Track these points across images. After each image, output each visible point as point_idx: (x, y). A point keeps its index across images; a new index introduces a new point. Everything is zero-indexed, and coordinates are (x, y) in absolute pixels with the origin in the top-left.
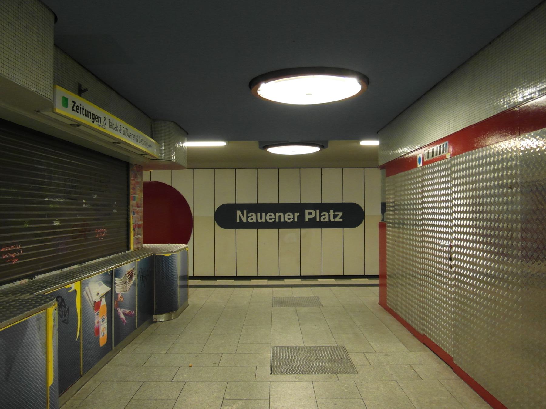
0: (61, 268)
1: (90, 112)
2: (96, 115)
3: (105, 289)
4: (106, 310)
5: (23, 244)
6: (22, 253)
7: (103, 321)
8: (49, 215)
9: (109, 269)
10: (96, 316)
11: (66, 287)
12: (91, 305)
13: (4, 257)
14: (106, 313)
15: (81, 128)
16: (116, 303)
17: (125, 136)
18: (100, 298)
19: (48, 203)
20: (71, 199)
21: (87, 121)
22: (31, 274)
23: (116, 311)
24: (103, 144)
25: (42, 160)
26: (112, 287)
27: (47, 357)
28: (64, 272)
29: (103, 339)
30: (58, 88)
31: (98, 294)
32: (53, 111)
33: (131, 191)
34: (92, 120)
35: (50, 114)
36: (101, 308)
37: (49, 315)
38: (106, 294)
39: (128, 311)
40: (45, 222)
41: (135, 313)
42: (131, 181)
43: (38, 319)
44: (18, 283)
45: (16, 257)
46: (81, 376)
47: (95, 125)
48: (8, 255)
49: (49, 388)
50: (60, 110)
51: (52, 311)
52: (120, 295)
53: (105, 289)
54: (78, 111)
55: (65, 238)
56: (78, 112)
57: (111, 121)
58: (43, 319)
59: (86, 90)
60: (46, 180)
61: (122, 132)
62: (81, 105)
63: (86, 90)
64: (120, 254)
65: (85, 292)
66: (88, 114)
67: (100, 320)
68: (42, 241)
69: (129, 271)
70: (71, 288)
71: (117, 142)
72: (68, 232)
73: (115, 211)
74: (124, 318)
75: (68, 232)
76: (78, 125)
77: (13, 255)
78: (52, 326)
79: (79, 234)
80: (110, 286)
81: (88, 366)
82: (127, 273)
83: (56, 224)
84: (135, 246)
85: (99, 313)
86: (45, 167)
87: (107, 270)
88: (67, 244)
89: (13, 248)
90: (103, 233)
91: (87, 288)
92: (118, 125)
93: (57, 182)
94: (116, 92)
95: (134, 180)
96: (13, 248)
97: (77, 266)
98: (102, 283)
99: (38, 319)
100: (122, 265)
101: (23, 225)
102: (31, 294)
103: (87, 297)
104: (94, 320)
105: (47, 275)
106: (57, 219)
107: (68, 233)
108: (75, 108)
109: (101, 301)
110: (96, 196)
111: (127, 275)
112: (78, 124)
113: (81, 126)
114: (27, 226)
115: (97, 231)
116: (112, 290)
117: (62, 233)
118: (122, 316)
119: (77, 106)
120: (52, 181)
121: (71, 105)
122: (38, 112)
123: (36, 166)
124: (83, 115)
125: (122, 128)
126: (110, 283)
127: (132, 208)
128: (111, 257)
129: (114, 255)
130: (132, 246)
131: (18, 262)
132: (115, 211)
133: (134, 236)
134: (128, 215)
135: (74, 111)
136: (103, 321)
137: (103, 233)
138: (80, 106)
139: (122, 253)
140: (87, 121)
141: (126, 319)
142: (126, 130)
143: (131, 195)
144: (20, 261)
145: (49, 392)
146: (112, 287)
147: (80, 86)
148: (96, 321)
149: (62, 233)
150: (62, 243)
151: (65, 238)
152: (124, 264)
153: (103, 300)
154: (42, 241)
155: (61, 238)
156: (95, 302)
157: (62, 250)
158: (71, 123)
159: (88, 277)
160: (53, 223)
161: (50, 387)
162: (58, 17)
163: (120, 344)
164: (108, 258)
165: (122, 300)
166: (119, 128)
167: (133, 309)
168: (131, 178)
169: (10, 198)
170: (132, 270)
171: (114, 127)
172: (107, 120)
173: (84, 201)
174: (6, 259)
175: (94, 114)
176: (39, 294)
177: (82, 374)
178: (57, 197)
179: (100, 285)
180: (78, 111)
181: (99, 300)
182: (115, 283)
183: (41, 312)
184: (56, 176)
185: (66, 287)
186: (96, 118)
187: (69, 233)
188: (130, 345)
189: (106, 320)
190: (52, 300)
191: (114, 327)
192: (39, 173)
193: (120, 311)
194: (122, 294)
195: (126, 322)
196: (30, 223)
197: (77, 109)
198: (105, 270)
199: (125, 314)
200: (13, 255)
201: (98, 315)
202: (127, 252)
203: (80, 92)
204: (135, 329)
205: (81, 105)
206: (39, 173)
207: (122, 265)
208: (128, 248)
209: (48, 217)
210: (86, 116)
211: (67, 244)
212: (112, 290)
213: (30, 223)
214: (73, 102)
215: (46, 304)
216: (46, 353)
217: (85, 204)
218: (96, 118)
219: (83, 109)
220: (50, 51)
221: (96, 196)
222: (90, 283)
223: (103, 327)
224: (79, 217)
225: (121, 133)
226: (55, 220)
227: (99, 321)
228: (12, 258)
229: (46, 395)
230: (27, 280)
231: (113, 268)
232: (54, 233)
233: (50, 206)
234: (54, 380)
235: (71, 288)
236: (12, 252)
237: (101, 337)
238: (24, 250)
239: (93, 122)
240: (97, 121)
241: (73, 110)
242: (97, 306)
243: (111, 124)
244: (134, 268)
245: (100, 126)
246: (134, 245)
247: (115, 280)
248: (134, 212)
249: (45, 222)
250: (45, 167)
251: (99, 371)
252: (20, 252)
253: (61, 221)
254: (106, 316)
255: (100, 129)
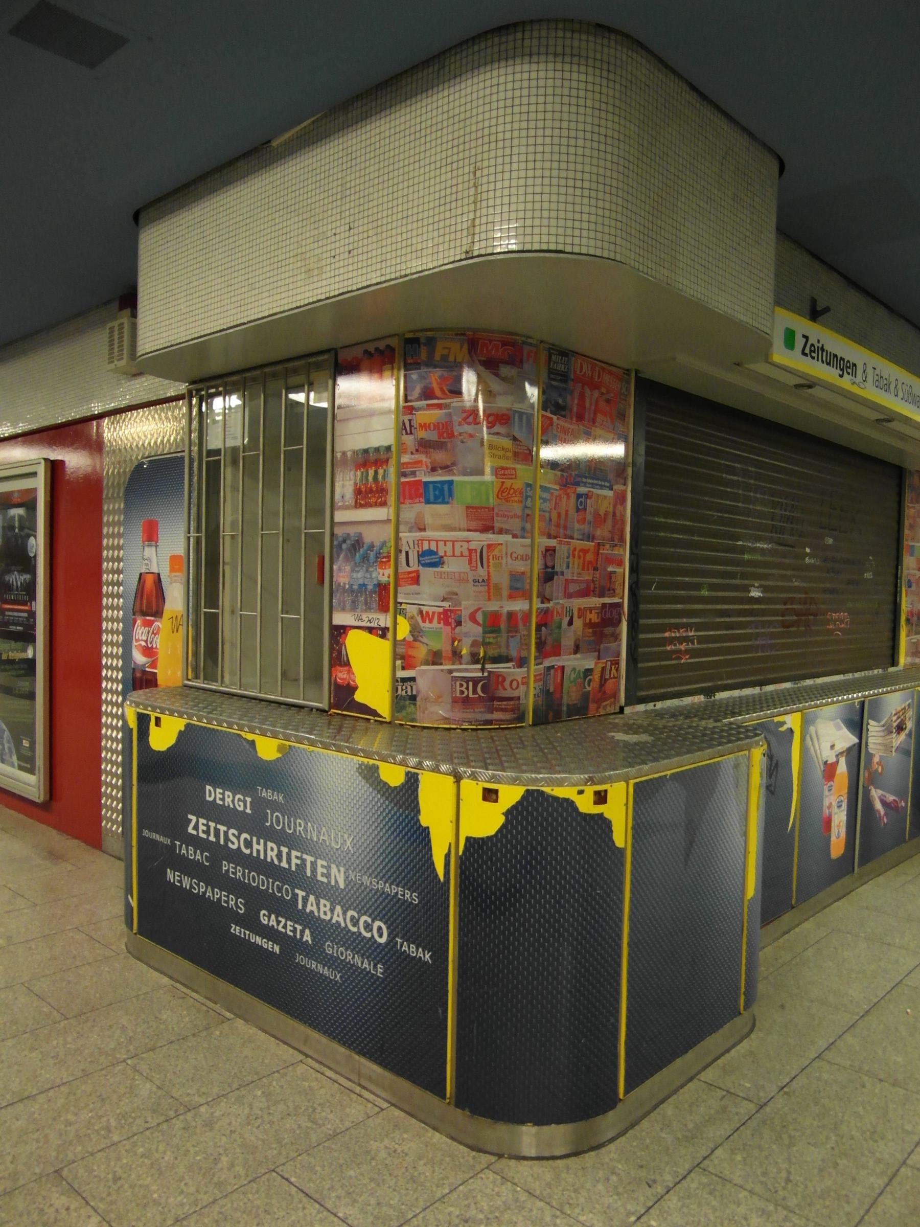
0: (761, 684)
1: (835, 356)
2: (848, 361)
3: (846, 739)
4: (847, 785)
5: (699, 627)
6: (696, 646)
7: (839, 807)
8: (744, 576)
9: (858, 697)
10: (826, 792)
11: (776, 719)
12: (819, 770)
13: (669, 648)
14: (846, 791)
15: (816, 392)
16: (867, 775)
17: (907, 404)
18: (837, 756)
19: (743, 550)
20: (785, 545)
21: (828, 374)
22: (709, 687)
23: (867, 793)
24: (856, 427)
25: (736, 465)
26: (860, 738)
27: (746, 842)
28: (766, 693)
29: (837, 847)
30: (780, 312)
31: (832, 747)
32: (767, 359)
33: (906, 532)
34: (839, 372)
35: (761, 368)
36: (837, 779)
37: (754, 763)
38: (849, 750)
39: (890, 798)
40: (736, 588)
41: (906, 804)
42: (907, 511)
43: (737, 766)
44: (688, 700)
45: (687, 652)
46: (793, 908)
47: (846, 383)
48: (675, 645)
49: (746, 904)
50: (780, 356)
51: (758, 755)
52: (876, 759)
53: (846, 739)
54: (813, 354)
55: (770, 624)
56: (813, 358)
57: (877, 372)
58: (743, 768)
59: (827, 310)
60: (740, 505)
61: (901, 394)
62: (819, 341)
63: (827, 310)
64: (876, 672)
65: (808, 737)
66: (832, 360)
67: (834, 804)
68: (730, 626)
69: (899, 709)
70: (784, 723)
71: (887, 418)
72: (775, 613)
73: (868, 575)
74: (882, 812)
75: (775, 613)
76: (810, 387)
77: (683, 647)
78: (758, 785)
79: (795, 618)
80: (857, 732)
81: (805, 895)
82: (894, 712)
83: (755, 593)
84: (909, 660)
85: (833, 788)
86: (740, 479)
87: (853, 699)
88: (772, 636)
89: (682, 633)
90: (842, 621)
91: (812, 729)
92: (893, 380)
93: (758, 508)
94: (886, 306)
95: (914, 508)
96: (682, 633)
97: (787, 685)
98: (842, 725)
99: (737, 766)
100: (883, 693)
101: (699, 590)
102: (716, 721)
103: (812, 748)
104: (822, 801)
105: (736, 693)
106: (757, 585)
107: (774, 615)
108: (807, 351)
109: (837, 762)
110: (830, 541)
111: (894, 718)
112: (810, 384)
113: (817, 387)
114: (705, 593)
115: (831, 616)
116: (860, 744)
117: (763, 613)
118: (878, 806)
119: (812, 345)
120: (751, 507)
121: (799, 342)
122: (738, 365)
123: (724, 475)
124: (823, 362)
125: (899, 386)
126: (857, 724)
127: (905, 572)
128: (857, 675)
129: (863, 673)
130: (903, 660)
131: (689, 661)
132: (868, 575)
133: (908, 636)
134: (896, 586)
135: (806, 355)
136: (839, 807)
137: (842, 621)
138: (816, 345)
139: (880, 671)
140: (828, 374)
141: (886, 814)
142: (908, 388)
143: (905, 543)
144: (692, 660)
145: (746, 910)
146: (860, 738)
147: (814, 302)
148: (826, 803)
149: (763, 613)
150: (763, 634)
151: (770, 624)
152: (887, 692)
153: (843, 760)
154: (730, 626)
155: (764, 624)
156: (826, 763)
157: (763, 648)
158: (797, 383)
159: (817, 706)
160: (749, 591)
161: (749, 901)
162: (786, 162)
163: (869, 866)
164: (849, 676)
165: (880, 769)
166: (892, 387)
167: (903, 797)
168: (907, 504)
169: (675, 536)
170: (905, 708)
171: (883, 384)
172: (870, 371)
173: (808, 550)
174: (673, 652)
175: (843, 360)
176: (731, 723)
177: (793, 902)
178: (759, 539)
179: (839, 729)
180: (813, 354)
181: (834, 760)
182: (868, 730)
183: (741, 753)
184: (758, 496)
185: (776, 719)
186: (846, 367)
187: (777, 615)
188: (890, 873)
189: (844, 806)
190: (756, 735)
191: (861, 827)
192: (729, 490)
193: (875, 793)
194: (881, 756)
195: (885, 820)
196: (712, 587)
197: (811, 351)
198: (848, 700)
199: (884, 803)
200: (683, 647)
201: (830, 790)
202: (891, 669)
203: (815, 314)
204: (905, 842)
205: (819, 341)
206: (729, 490)
207: (883, 693)
208: (894, 662)
209: (742, 578)
210: (828, 364)
211: (772, 636)
212: (860, 744)
213: (712, 587)
214: (804, 336)
215: (748, 741)
216: (745, 834)
217: (811, 556)
218: (846, 367)
219: (823, 350)
220: (770, 236)
221: (830, 541)
222: (819, 720)
223: (840, 818)
224: (796, 584)
225: (896, 396)
226: (754, 586)
227: (831, 804)
228: (680, 651)
229: (742, 914)
230: (702, 698)
231: (866, 697)
232: (751, 613)
233: (746, 557)
234: (755, 890)
235: (784, 723)
236: (681, 640)
237: (833, 838)
238: (701, 640)
239: (841, 376)
240: (848, 374)
241: (804, 354)
242: (830, 770)
243: (876, 378)
244: (909, 705)
245: (854, 383)
246: (906, 655)
247: (868, 724)
248: (909, 581)
249: (736, 588)
250: (740, 479)
251: (825, 907)
252: (693, 643)
253: (765, 589)
254: (846, 796)
255: (855, 390)
